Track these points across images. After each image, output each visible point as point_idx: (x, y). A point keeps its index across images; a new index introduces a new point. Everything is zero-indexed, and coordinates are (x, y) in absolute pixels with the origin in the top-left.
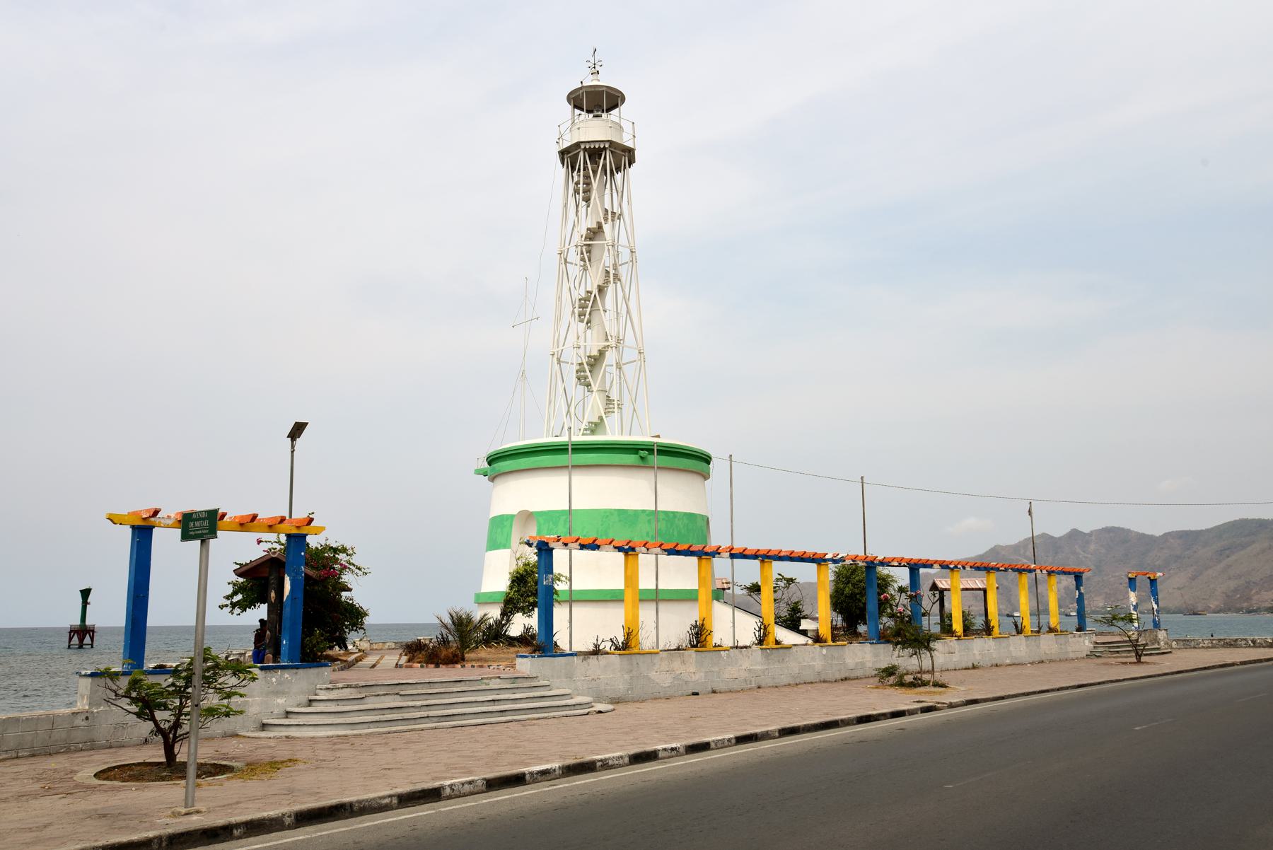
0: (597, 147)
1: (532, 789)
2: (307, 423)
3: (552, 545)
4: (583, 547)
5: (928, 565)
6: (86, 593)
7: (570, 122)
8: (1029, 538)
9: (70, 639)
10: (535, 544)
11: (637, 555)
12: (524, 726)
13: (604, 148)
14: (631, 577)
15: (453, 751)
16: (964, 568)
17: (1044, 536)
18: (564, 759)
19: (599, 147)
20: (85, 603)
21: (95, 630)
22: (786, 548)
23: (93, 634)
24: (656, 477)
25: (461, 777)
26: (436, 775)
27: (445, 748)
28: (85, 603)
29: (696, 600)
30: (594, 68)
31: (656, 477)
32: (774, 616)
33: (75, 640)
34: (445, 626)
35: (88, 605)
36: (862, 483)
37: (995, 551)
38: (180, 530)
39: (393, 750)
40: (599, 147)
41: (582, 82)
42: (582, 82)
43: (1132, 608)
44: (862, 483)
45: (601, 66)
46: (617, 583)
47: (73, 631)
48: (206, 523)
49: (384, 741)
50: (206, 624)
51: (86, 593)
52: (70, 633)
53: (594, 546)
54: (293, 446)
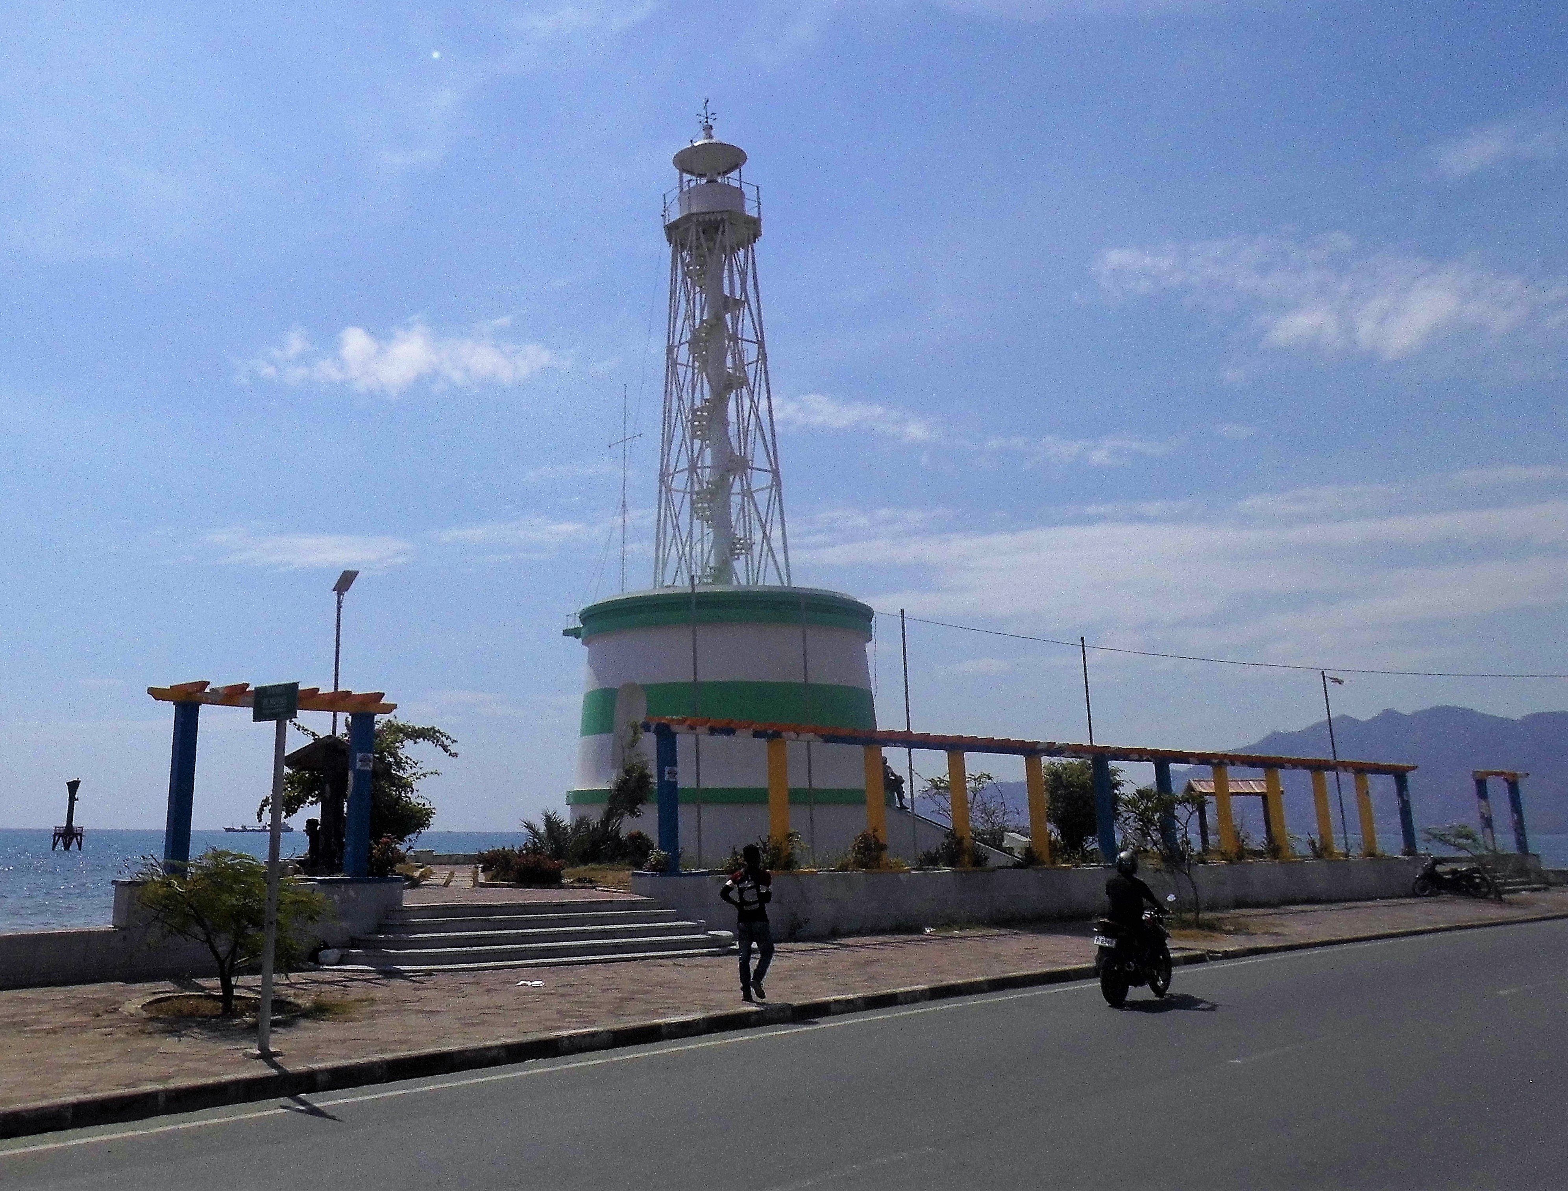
0: (712, 219)
1: (600, 1058)
2: (358, 572)
3: (675, 728)
4: (713, 731)
5: (1181, 757)
6: (73, 787)
7: (678, 190)
8: (1319, 725)
9: (55, 844)
10: (653, 727)
11: (785, 742)
12: (647, 966)
13: (723, 220)
14: (777, 768)
15: (563, 995)
16: (425, 776)
17: (1344, 718)
18: (711, 1008)
19: (716, 219)
20: (72, 799)
21: (83, 834)
22: (982, 734)
23: (81, 839)
24: (694, 632)
25: (579, 1028)
26: (548, 1024)
27: (553, 991)
28: (72, 799)
29: (765, 802)
30: (707, 122)
31: (694, 632)
32: (1506, 784)
33: (60, 846)
34: (536, 833)
35: (76, 802)
36: (1083, 646)
37: (1275, 738)
38: (252, 709)
39: (488, 991)
40: (716, 219)
41: (691, 141)
42: (691, 141)
43: (1080, 855)
44: (1083, 646)
45: (715, 119)
46: (759, 780)
47: (57, 834)
48: (283, 701)
49: (474, 979)
50: (1369, 776)
51: (73, 787)
52: (54, 836)
53: (729, 731)
54: (339, 603)
